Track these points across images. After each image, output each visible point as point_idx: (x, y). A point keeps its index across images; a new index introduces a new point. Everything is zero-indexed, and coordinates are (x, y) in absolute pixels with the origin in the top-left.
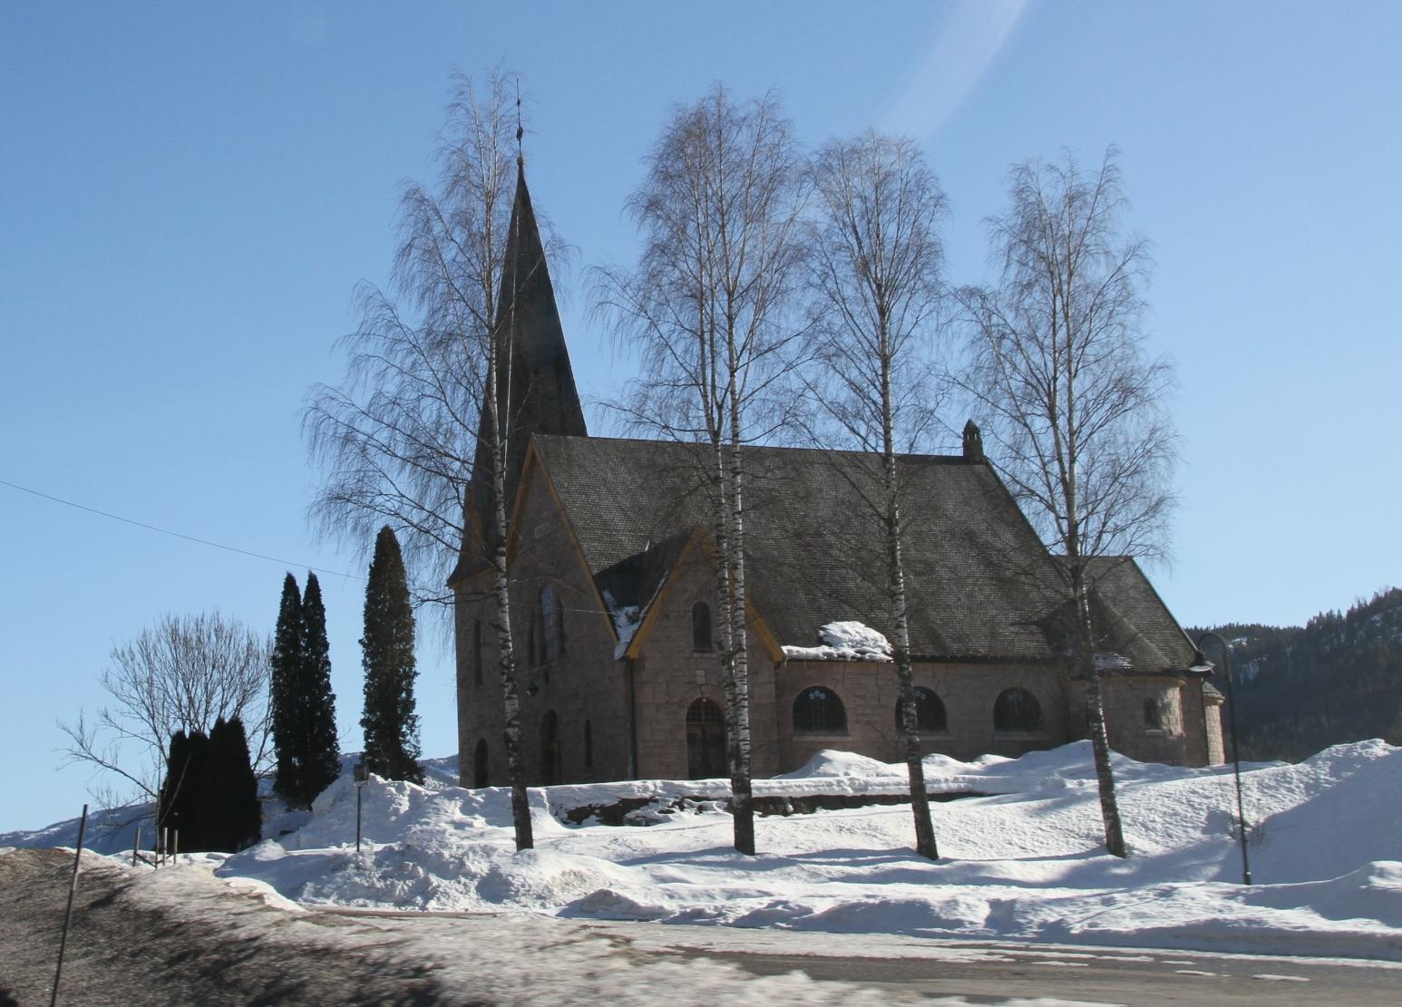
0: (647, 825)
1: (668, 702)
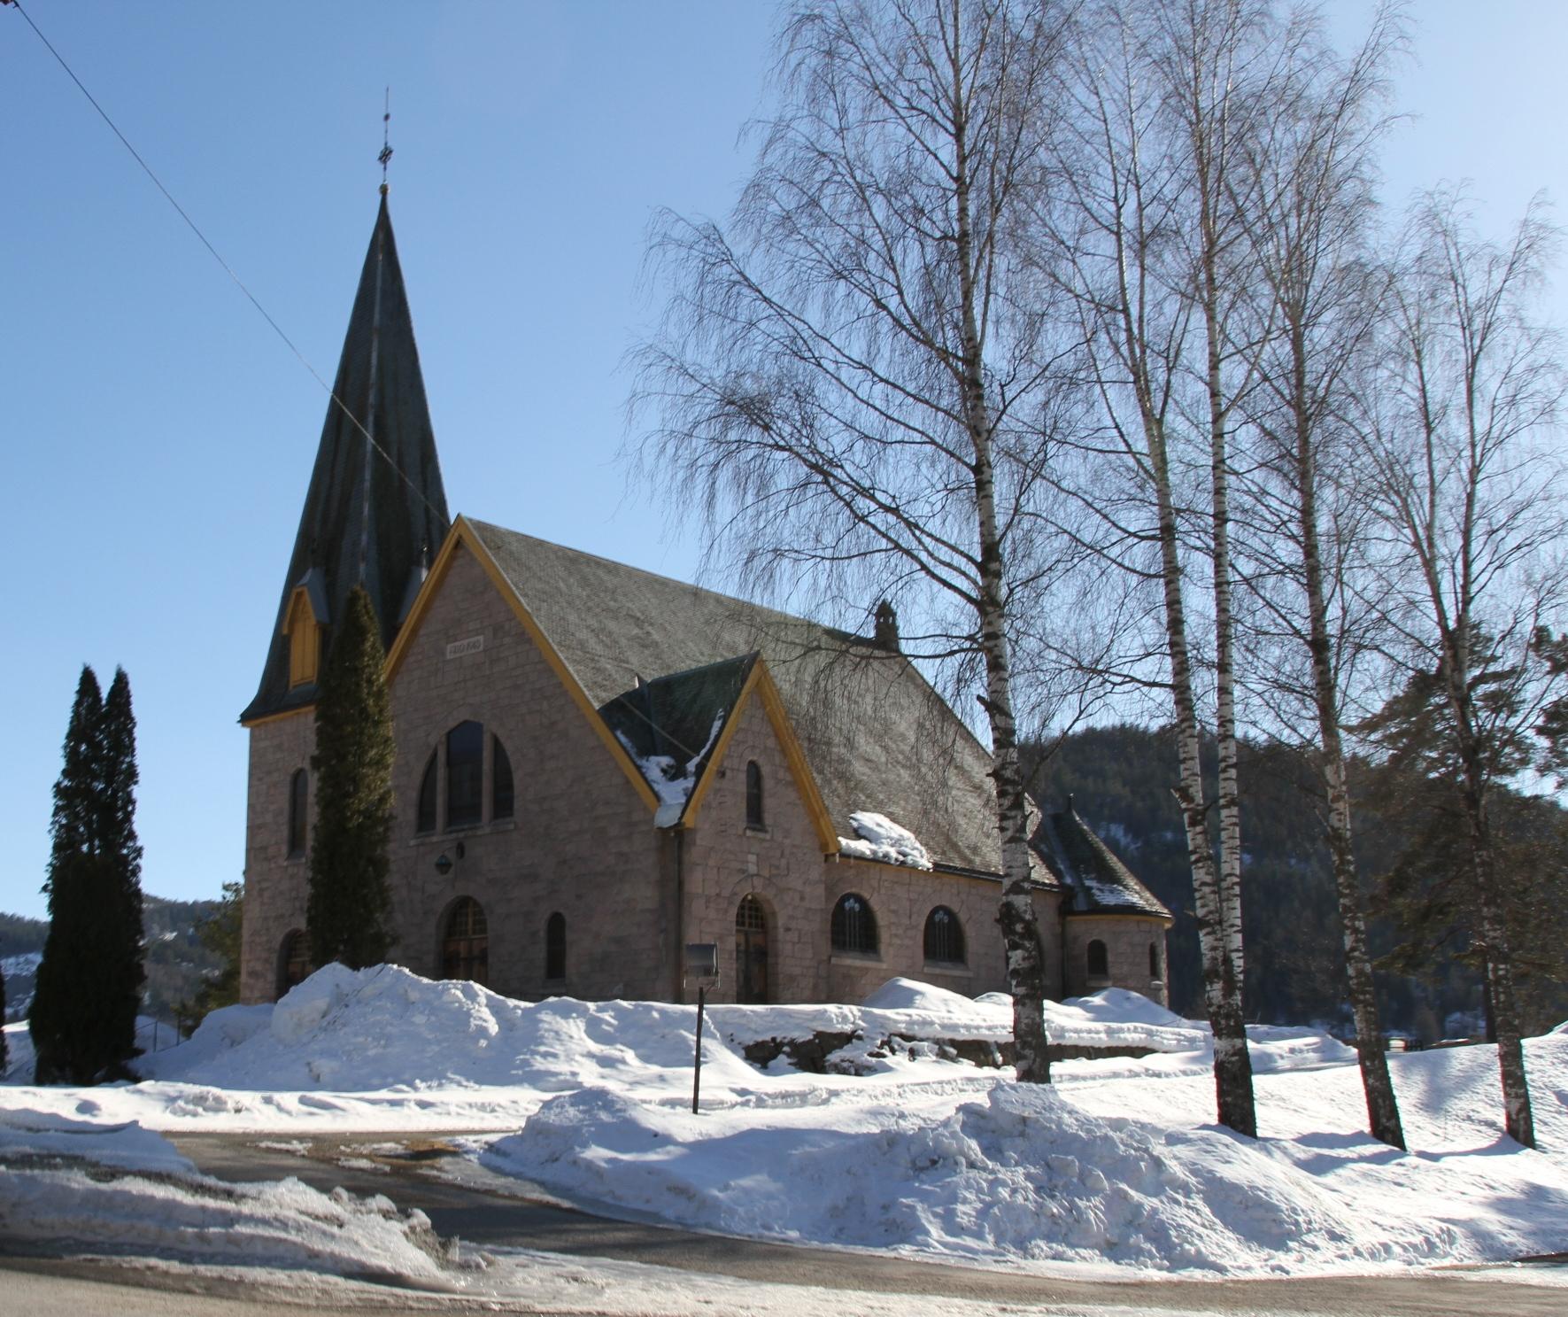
0: (858, 1074)
1: (718, 895)
